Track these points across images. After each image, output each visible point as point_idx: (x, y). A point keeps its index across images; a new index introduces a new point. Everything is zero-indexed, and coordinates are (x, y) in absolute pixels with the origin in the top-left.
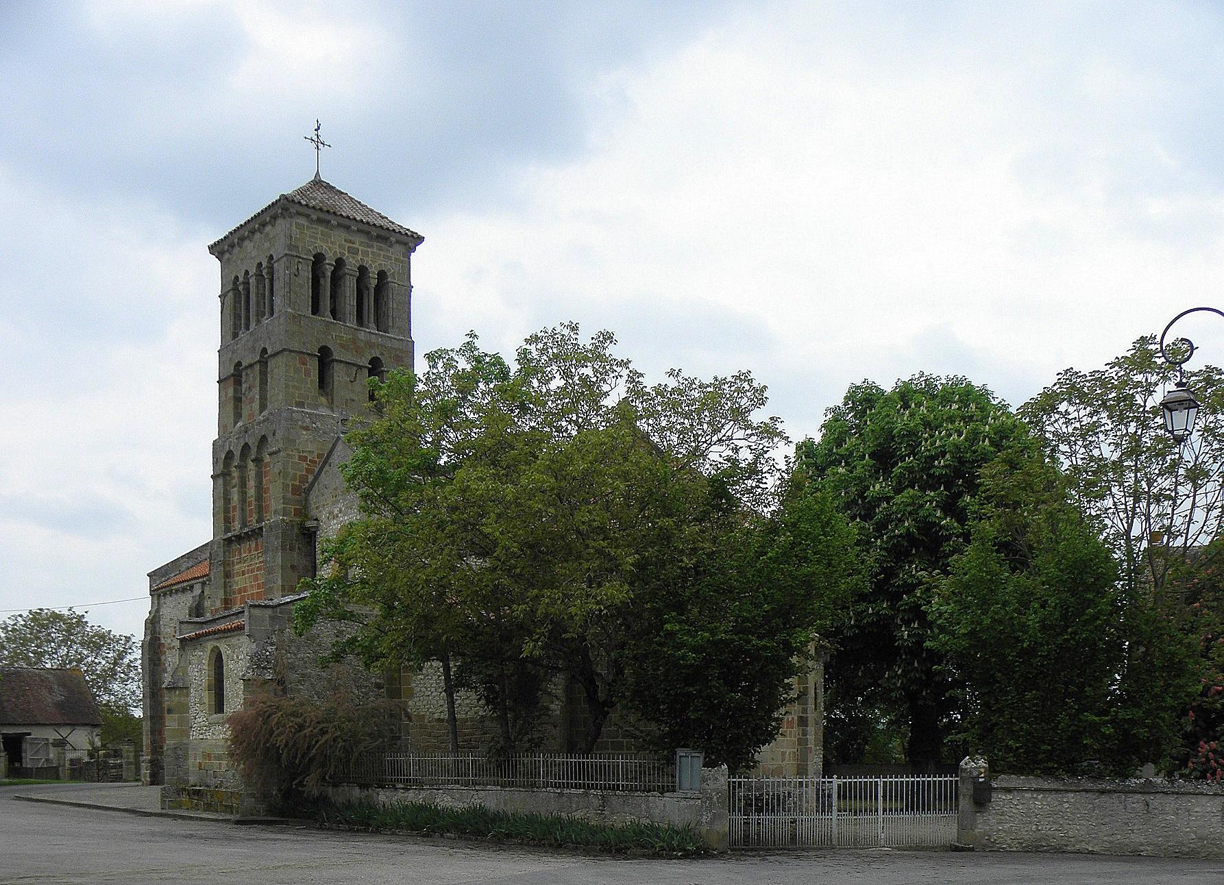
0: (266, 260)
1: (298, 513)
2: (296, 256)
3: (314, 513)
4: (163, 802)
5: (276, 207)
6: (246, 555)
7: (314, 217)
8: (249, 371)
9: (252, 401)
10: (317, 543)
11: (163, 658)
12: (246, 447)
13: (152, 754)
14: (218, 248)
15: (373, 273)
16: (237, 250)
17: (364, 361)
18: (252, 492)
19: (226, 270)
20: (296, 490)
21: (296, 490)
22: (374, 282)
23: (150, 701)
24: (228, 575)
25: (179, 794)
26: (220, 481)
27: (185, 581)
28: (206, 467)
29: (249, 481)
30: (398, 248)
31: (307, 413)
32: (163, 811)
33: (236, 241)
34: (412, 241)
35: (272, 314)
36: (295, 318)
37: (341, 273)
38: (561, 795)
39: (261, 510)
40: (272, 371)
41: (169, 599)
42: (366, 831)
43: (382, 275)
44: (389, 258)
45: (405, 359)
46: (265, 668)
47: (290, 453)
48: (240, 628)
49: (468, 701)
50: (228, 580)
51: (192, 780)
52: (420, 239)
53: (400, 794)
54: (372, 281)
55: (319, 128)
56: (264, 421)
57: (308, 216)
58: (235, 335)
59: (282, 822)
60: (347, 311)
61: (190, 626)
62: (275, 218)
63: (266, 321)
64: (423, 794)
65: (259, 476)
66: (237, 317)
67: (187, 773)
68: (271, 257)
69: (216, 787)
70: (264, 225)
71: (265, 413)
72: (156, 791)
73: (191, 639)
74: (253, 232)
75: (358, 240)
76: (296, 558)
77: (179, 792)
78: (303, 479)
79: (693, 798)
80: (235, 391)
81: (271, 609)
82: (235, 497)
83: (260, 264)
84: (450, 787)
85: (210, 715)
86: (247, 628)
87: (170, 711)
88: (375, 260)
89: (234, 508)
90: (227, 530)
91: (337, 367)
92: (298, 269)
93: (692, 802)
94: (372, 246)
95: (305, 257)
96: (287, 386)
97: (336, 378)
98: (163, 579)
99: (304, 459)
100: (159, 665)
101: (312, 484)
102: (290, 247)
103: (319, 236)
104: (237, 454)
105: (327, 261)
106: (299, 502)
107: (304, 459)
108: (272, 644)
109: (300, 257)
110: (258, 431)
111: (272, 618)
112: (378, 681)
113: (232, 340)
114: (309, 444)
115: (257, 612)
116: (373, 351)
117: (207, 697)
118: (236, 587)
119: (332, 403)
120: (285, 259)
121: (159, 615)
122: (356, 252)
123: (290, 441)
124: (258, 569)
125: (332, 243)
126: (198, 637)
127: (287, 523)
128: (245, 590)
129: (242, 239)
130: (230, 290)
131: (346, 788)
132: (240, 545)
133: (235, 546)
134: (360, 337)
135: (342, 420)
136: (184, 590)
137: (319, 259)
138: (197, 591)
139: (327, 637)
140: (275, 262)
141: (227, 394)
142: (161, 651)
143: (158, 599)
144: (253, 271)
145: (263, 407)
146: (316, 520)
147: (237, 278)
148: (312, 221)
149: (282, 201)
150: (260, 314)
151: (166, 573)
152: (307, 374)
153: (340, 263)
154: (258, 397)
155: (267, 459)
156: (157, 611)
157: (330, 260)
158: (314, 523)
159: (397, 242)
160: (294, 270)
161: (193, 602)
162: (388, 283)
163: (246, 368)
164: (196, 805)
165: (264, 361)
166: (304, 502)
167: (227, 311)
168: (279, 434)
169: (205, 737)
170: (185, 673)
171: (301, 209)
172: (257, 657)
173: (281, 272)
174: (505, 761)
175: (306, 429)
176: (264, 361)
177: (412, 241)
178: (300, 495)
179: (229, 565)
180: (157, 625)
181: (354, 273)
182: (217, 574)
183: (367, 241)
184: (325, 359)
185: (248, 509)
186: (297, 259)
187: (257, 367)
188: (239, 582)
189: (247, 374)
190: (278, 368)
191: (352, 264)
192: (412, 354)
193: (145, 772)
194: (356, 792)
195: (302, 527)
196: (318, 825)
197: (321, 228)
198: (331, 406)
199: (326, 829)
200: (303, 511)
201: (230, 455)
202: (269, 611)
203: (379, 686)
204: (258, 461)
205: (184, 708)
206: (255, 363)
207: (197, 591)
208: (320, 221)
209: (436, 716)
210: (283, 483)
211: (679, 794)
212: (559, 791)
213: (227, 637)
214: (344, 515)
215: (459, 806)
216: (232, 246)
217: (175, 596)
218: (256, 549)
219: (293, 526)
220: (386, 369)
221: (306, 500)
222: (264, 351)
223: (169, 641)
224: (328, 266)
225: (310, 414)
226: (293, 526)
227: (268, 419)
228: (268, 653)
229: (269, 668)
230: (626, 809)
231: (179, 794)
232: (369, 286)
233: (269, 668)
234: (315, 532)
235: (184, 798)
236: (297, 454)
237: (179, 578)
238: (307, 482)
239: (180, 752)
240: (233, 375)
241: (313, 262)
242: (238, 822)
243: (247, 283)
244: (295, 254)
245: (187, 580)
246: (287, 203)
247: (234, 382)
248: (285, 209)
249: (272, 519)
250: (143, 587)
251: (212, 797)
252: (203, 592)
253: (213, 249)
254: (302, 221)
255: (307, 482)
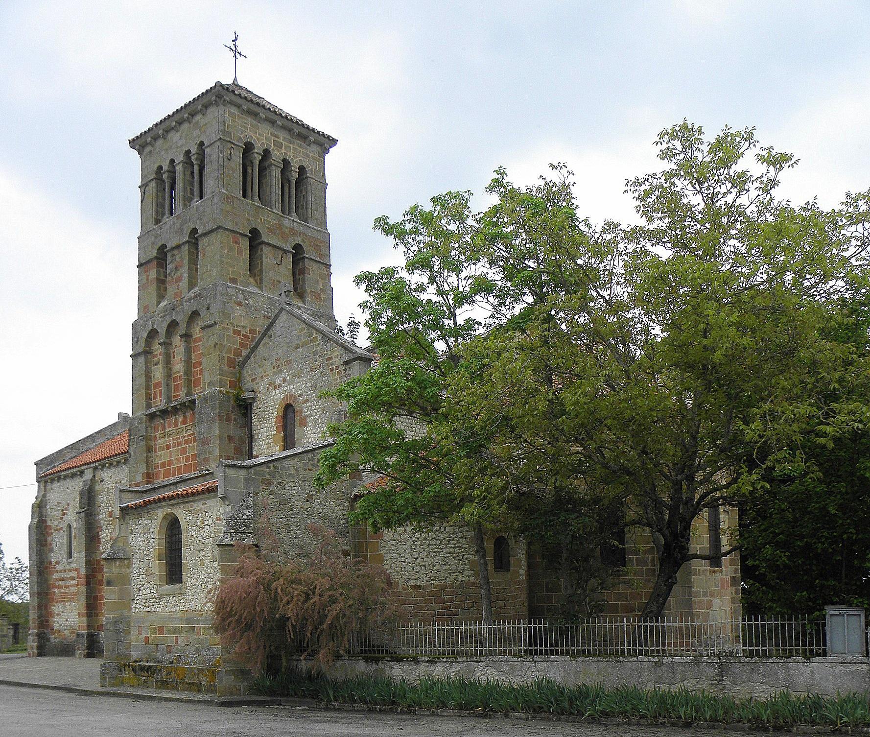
0: (196, 147)
1: (233, 385)
2: (230, 142)
3: (249, 385)
4: (103, 679)
5: (210, 94)
6: (170, 429)
7: (246, 108)
8: (175, 252)
9: (179, 279)
10: (253, 415)
11: (49, 539)
12: (173, 325)
13: (39, 628)
14: (140, 142)
15: (295, 167)
16: (160, 142)
17: (289, 247)
18: (178, 367)
19: (148, 163)
20: (231, 363)
21: (231, 363)
22: (296, 176)
23: (37, 578)
24: (149, 450)
25: (121, 670)
26: (142, 359)
27: (76, 467)
28: (126, 346)
29: (174, 358)
30: (314, 147)
31: (240, 289)
32: (104, 690)
33: (161, 132)
34: (326, 143)
35: (201, 198)
36: (229, 199)
37: (266, 164)
38: (659, 664)
39: (190, 384)
40: (204, 249)
41: (56, 485)
42: (392, 711)
43: (302, 169)
44: (308, 156)
45: (323, 249)
46: (243, 532)
47: (226, 326)
48: (214, 490)
49: (445, 567)
50: (150, 455)
51: (135, 655)
52: (333, 142)
53: (423, 668)
54: (294, 174)
55: (236, 39)
56: (195, 297)
57: (239, 106)
58: (158, 221)
59: (273, 703)
60: (274, 198)
61: (130, 495)
62: (206, 107)
63: (196, 203)
64: (456, 667)
65: (188, 351)
66: (160, 205)
67: (128, 647)
68: (202, 144)
69: (172, 663)
70: (193, 115)
71: (196, 289)
72: (94, 665)
73: (136, 507)
74: (180, 123)
75: (282, 135)
76: (233, 429)
77: (121, 668)
78: (238, 353)
79: (855, 663)
80: (158, 273)
81: (245, 470)
82: (158, 373)
83: (188, 152)
84: (496, 658)
85: (161, 586)
86: (221, 491)
87: (109, 583)
88: (298, 156)
89: (157, 385)
90: (149, 406)
91: (266, 250)
92: (231, 153)
93: (853, 668)
94: (294, 143)
95: (237, 143)
96: (222, 262)
97: (264, 259)
98: (49, 467)
99: (238, 333)
100: (46, 545)
101: (248, 357)
102: (224, 132)
103: (249, 126)
104: (162, 331)
105: (256, 151)
106: (235, 374)
107: (238, 333)
108: (248, 507)
109: (232, 143)
110: (188, 308)
111: (247, 480)
112: (345, 547)
113: (155, 225)
114: (243, 320)
115: (231, 472)
116: (296, 238)
117: (158, 568)
118: (158, 462)
119: (261, 282)
120: (218, 143)
121: (46, 500)
122: (280, 146)
123: (226, 315)
124: (186, 442)
125: (259, 134)
126: (146, 504)
127: (224, 394)
128: (170, 463)
129: (167, 131)
130: (152, 180)
131: (346, 662)
132: (164, 420)
133: (158, 422)
134: (285, 223)
135: (285, 292)
136: (73, 476)
137: (248, 148)
138: (88, 475)
139: (299, 501)
140: (206, 148)
141: (148, 277)
142: (47, 533)
143: (45, 486)
144: (179, 158)
145: (191, 285)
146: (253, 391)
147: (160, 168)
148: (243, 111)
149: (217, 88)
150: (187, 200)
151: (52, 462)
152: (240, 253)
153: (266, 153)
154: (186, 275)
155: (197, 332)
156: (44, 496)
157: (258, 149)
158: (252, 395)
159: (316, 142)
160: (227, 154)
161: (84, 486)
162: (307, 177)
163: (173, 249)
164: (144, 682)
165: (194, 238)
166: (238, 375)
167: (149, 200)
168: (213, 309)
169: (153, 610)
170: (126, 542)
171: (234, 98)
172: (234, 521)
173: (214, 156)
174: (572, 628)
175: (240, 304)
176: (194, 238)
177: (326, 143)
178: (234, 368)
179: (151, 440)
180: (44, 510)
181: (279, 165)
182: (137, 449)
183: (290, 138)
184: (254, 239)
185: (173, 384)
186: (229, 145)
187: (186, 248)
188: (161, 456)
189: (173, 256)
190: (211, 247)
191: (277, 155)
192: (328, 245)
193: (32, 643)
194: (361, 667)
195: (238, 398)
196: (322, 705)
197: (250, 120)
198: (260, 284)
199: (335, 710)
200: (237, 383)
201: (153, 334)
202: (244, 473)
203: (346, 553)
204: (187, 336)
205: (125, 580)
206: (183, 244)
207: (88, 475)
208: (250, 113)
209: (412, 583)
210: (219, 355)
211: (833, 658)
212: (656, 660)
213: (187, 502)
214: (290, 384)
215: (517, 681)
216: (155, 138)
217: (62, 482)
218: (185, 422)
219: (229, 397)
220: (307, 256)
221: (240, 373)
222: (194, 231)
223: (56, 523)
224: (256, 155)
225: (242, 291)
226: (229, 397)
227: (200, 295)
228: (245, 517)
229: (248, 533)
230: (756, 678)
231: (121, 670)
232: (291, 178)
233: (248, 533)
234: (251, 404)
235: (127, 674)
236: (232, 328)
237: (66, 466)
238: (241, 356)
239: (121, 626)
240: (156, 258)
241: (244, 150)
242: (223, 704)
243: (172, 172)
244: (228, 139)
245: (78, 466)
246: (222, 90)
247: (157, 265)
248: (219, 96)
249: (202, 391)
250: (32, 473)
251: (168, 673)
252: (94, 476)
253: (133, 143)
254: (234, 110)
255: (241, 356)
